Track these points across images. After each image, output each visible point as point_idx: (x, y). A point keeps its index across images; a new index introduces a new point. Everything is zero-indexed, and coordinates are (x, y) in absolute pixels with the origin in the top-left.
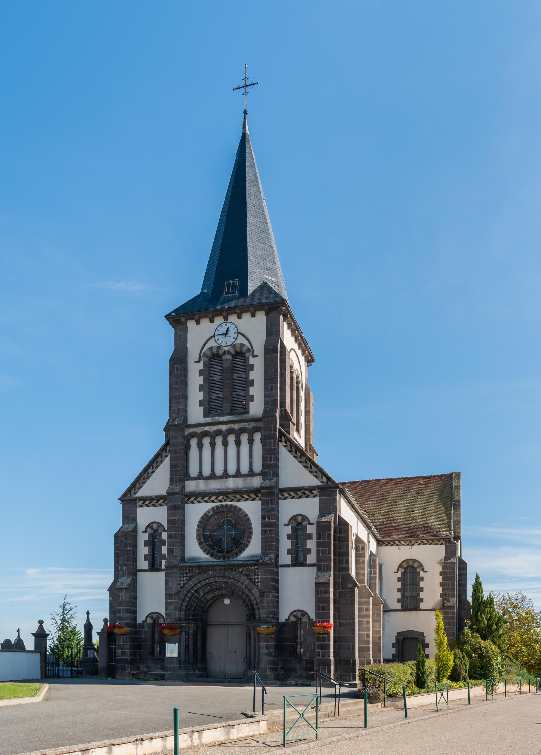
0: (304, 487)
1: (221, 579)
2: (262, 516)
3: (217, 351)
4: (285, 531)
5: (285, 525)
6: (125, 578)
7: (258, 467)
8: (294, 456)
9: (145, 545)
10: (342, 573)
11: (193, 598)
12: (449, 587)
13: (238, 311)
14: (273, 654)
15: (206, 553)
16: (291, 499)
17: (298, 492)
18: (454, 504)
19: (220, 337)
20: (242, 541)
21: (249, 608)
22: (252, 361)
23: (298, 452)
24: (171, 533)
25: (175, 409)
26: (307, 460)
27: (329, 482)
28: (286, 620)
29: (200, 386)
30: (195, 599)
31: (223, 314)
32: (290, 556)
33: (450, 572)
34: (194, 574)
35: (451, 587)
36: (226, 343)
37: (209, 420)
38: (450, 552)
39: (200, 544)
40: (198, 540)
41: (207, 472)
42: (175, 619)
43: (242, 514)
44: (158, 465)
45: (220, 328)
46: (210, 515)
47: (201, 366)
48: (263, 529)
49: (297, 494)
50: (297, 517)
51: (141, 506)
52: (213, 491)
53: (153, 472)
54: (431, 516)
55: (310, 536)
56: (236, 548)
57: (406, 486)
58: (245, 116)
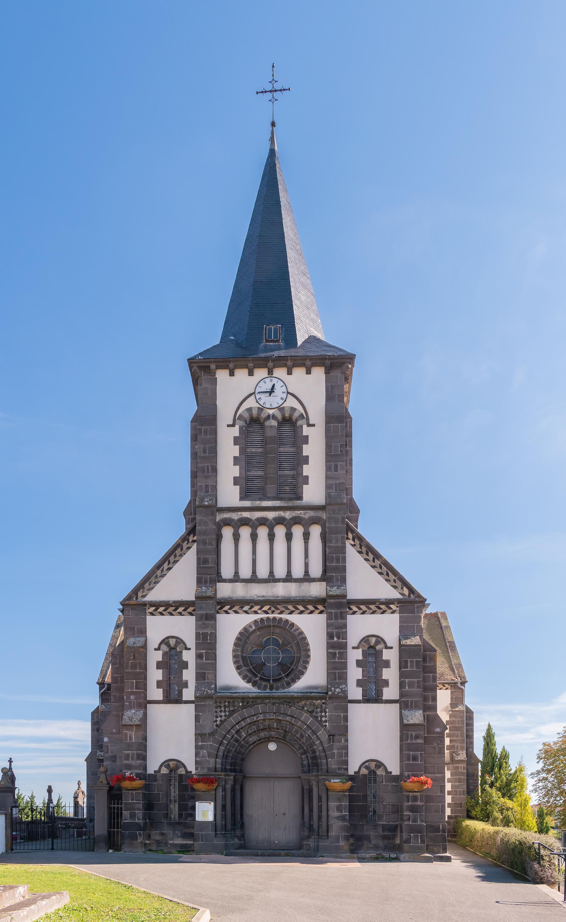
0: (380, 599)
1: (273, 716)
2: (328, 633)
3: (258, 414)
5: (354, 648)
6: (133, 711)
7: (316, 570)
8: (364, 559)
10: (427, 713)
11: (232, 741)
13: (289, 363)
14: (347, 818)
15: (246, 681)
17: (370, 606)
19: (262, 396)
20: (294, 666)
21: (307, 756)
22: (306, 431)
23: (370, 554)
24: (202, 651)
26: (382, 565)
27: (412, 595)
28: (355, 772)
29: (235, 458)
30: (234, 742)
31: (268, 364)
32: (361, 689)
33: (459, 721)
34: (236, 708)
35: (460, 738)
37: (247, 504)
38: (456, 698)
39: (238, 668)
40: (235, 663)
42: (209, 769)
43: (295, 630)
44: (176, 559)
45: (262, 384)
46: (251, 630)
47: (236, 431)
48: (331, 651)
49: (370, 609)
50: (370, 638)
51: (152, 614)
52: (255, 598)
53: (169, 569)
55: (387, 664)
56: (287, 676)
58: (273, 130)
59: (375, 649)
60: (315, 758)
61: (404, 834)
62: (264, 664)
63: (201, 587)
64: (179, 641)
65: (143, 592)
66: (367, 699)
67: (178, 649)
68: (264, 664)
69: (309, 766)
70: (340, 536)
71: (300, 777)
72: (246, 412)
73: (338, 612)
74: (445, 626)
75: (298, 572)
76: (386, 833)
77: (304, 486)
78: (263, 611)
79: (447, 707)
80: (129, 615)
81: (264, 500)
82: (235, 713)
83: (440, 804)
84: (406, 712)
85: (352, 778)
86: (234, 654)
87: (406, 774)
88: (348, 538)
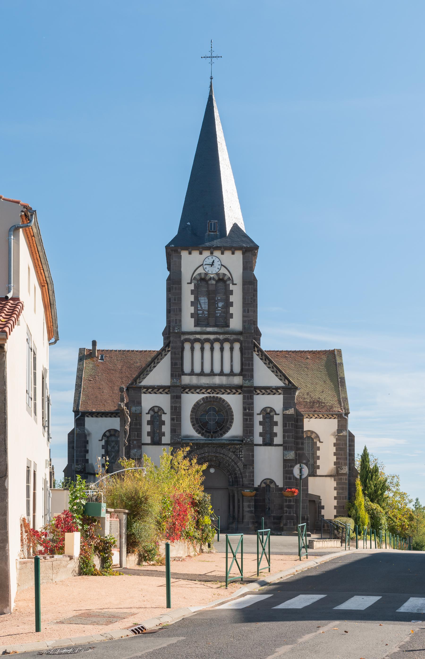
0: (272, 387)
1: (213, 454)
4: (258, 418)
5: (258, 414)
6: (135, 450)
7: (237, 369)
9: (148, 424)
10: (299, 452)
12: (342, 457)
15: (198, 432)
16: (262, 395)
18: (340, 381)
21: (232, 477)
22: (232, 287)
23: (267, 360)
24: (174, 416)
25: (174, 319)
26: (274, 367)
27: (290, 384)
28: (258, 486)
29: (192, 302)
32: (262, 438)
33: (342, 443)
34: (193, 449)
35: (343, 456)
36: (212, 272)
37: (198, 329)
39: (193, 425)
40: (192, 422)
41: (197, 369)
43: (225, 404)
44: (159, 361)
45: (207, 259)
46: (201, 403)
47: (192, 287)
48: (245, 417)
49: (267, 392)
50: (267, 409)
51: (145, 393)
52: (204, 385)
53: (155, 367)
54: (323, 392)
55: (276, 424)
56: (221, 430)
57: (296, 360)
59: (270, 414)
60: (236, 477)
61: (284, 521)
62: (207, 422)
63: (173, 379)
64: (160, 409)
65: (139, 380)
66: (265, 444)
67: (159, 414)
68: (207, 422)
69: (233, 482)
70: (250, 351)
71: (227, 488)
72: (198, 275)
73: (249, 396)
74: (339, 363)
75: (227, 370)
76: (275, 521)
77: (230, 319)
78: (208, 392)
79: (335, 433)
80: (131, 393)
81: (208, 327)
82: (193, 452)
83: (306, 504)
84: (286, 452)
85: (256, 489)
86: (191, 417)
87: (285, 487)
88: (255, 351)
